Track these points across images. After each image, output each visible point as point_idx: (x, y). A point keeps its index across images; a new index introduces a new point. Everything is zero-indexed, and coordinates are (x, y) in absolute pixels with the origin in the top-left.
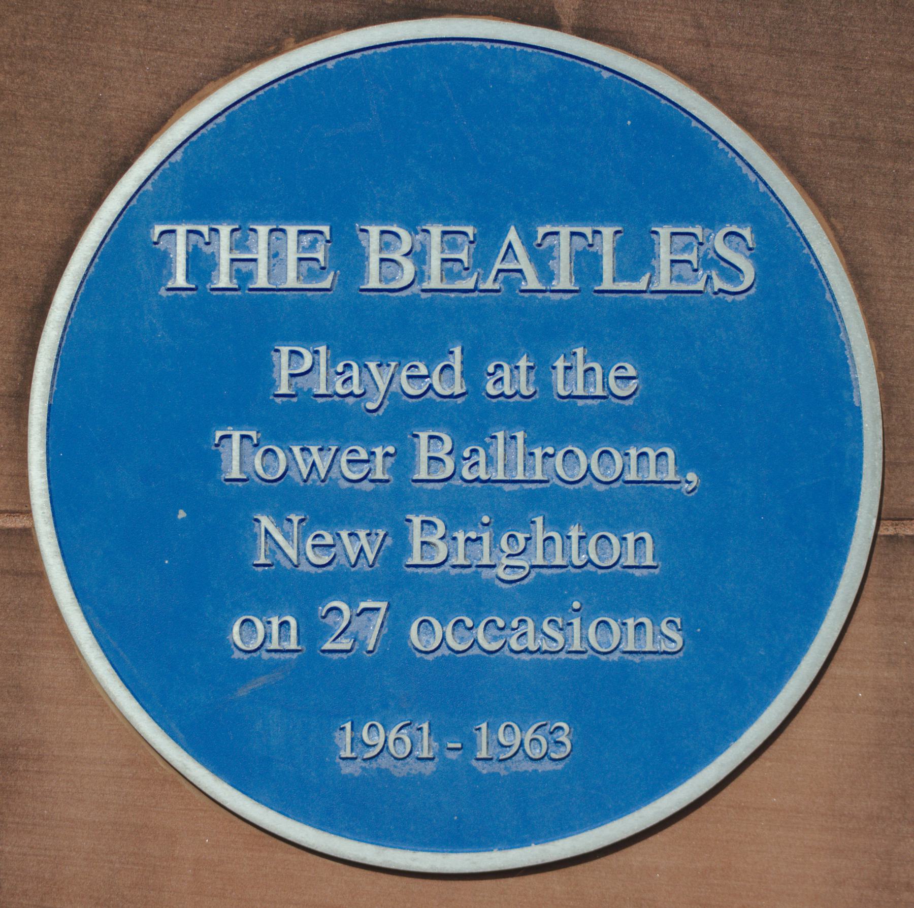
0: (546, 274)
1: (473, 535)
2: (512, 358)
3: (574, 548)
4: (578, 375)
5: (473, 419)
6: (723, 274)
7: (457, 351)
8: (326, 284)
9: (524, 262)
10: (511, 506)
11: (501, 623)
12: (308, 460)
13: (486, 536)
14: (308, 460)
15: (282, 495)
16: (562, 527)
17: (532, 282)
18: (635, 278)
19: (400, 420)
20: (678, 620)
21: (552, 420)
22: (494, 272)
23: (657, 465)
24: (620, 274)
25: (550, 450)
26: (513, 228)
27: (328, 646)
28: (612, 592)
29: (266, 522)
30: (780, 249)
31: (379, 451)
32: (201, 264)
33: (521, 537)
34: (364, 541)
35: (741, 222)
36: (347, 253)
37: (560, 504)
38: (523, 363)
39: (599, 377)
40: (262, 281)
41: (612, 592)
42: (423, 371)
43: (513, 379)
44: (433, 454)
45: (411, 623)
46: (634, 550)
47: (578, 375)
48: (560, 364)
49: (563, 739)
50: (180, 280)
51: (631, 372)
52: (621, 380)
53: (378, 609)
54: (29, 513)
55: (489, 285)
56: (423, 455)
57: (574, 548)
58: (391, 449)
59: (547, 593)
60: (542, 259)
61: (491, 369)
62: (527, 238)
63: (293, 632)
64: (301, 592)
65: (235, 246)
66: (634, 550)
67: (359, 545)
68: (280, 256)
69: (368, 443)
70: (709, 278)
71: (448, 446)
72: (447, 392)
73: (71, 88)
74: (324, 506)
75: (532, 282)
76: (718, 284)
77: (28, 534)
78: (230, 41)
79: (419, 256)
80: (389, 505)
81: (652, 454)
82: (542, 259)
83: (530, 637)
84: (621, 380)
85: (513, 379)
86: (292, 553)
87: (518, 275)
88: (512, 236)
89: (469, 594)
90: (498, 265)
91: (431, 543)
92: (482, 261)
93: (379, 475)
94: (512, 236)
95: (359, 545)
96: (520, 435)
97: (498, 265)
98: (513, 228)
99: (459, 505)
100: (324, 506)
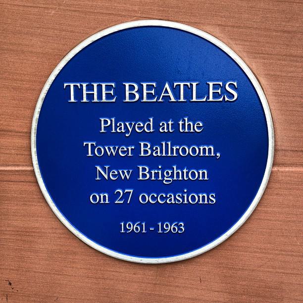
0: (177, 96)
2: (167, 121)
3: (185, 174)
4: (188, 125)
5: (155, 138)
6: (229, 97)
7: (151, 119)
8: (114, 100)
9: (170, 94)
10: (167, 163)
12: (111, 150)
13: (160, 172)
14: (111, 150)
15: (104, 160)
17: (173, 99)
19: (135, 139)
20: (214, 195)
21: (177, 138)
23: (207, 150)
24: (197, 97)
25: (178, 147)
28: (195, 186)
29: (98, 168)
31: (130, 148)
32: (79, 92)
34: (126, 173)
35: (234, 81)
36: (120, 91)
38: (170, 123)
41: (195, 186)
42: (142, 125)
43: (166, 127)
44: (145, 148)
46: (202, 174)
47: (188, 125)
48: (181, 123)
49: (182, 227)
51: (201, 125)
52: (196, 127)
55: (160, 100)
57: (185, 174)
58: (133, 147)
59: (177, 186)
61: (161, 124)
63: (107, 199)
64: (107, 186)
66: (202, 174)
67: (125, 174)
68: (100, 92)
69: (127, 146)
74: (115, 162)
75: (173, 99)
76: (226, 99)
77: (33, 172)
78: (84, 18)
79: (140, 91)
80: (132, 162)
81: (207, 148)
83: (173, 199)
84: (196, 127)
85: (166, 127)
86: (106, 177)
88: (167, 86)
89: (154, 186)
90: (163, 94)
91: (144, 173)
92: (158, 93)
94: (167, 86)
99: (152, 162)
100: (115, 162)
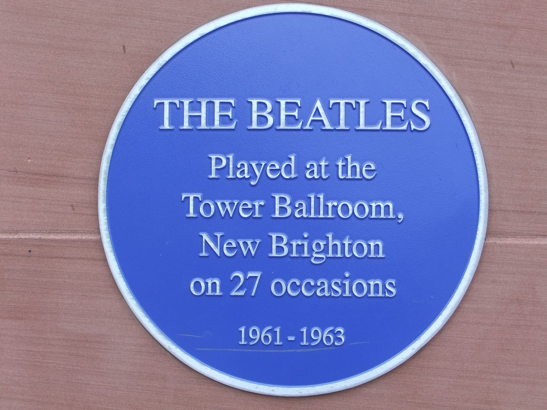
1: (300, 243)
3: (347, 247)
5: (299, 188)
8: (233, 127)
11: (312, 284)
12: (224, 207)
13: (306, 244)
14: (224, 207)
15: (214, 223)
16: (341, 239)
17: (328, 126)
18: (375, 124)
19: (266, 188)
22: (310, 121)
25: (335, 204)
26: (318, 101)
27: (233, 293)
28: (364, 268)
29: (205, 237)
30: (442, 107)
33: (322, 244)
35: (424, 98)
36: (243, 111)
37: (342, 227)
39: (358, 170)
40: (203, 125)
41: (364, 268)
42: (277, 167)
45: (269, 326)
50: (166, 125)
51: (373, 167)
53: (257, 277)
54: (99, 233)
55: (307, 127)
56: (277, 206)
57: (347, 247)
60: (333, 111)
62: (326, 104)
65: (191, 109)
66: (374, 247)
69: (252, 200)
70: (409, 124)
71: (288, 202)
72: (288, 177)
73: (117, 38)
74: (232, 226)
77: (100, 243)
80: (262, 226)
82: (333, 111)
83: (327, 288)
85: (317, 169)
86: (217, 251)
87: (320, 123)
88: (318, 104)
90: (311, 118)
92: (304, 117)
93: (257, 215)
95: (249, 247)
96: (321, 196)
97: (311, 118)
98: (318, 101)
99: (293, 226)
100: (232, 226)
